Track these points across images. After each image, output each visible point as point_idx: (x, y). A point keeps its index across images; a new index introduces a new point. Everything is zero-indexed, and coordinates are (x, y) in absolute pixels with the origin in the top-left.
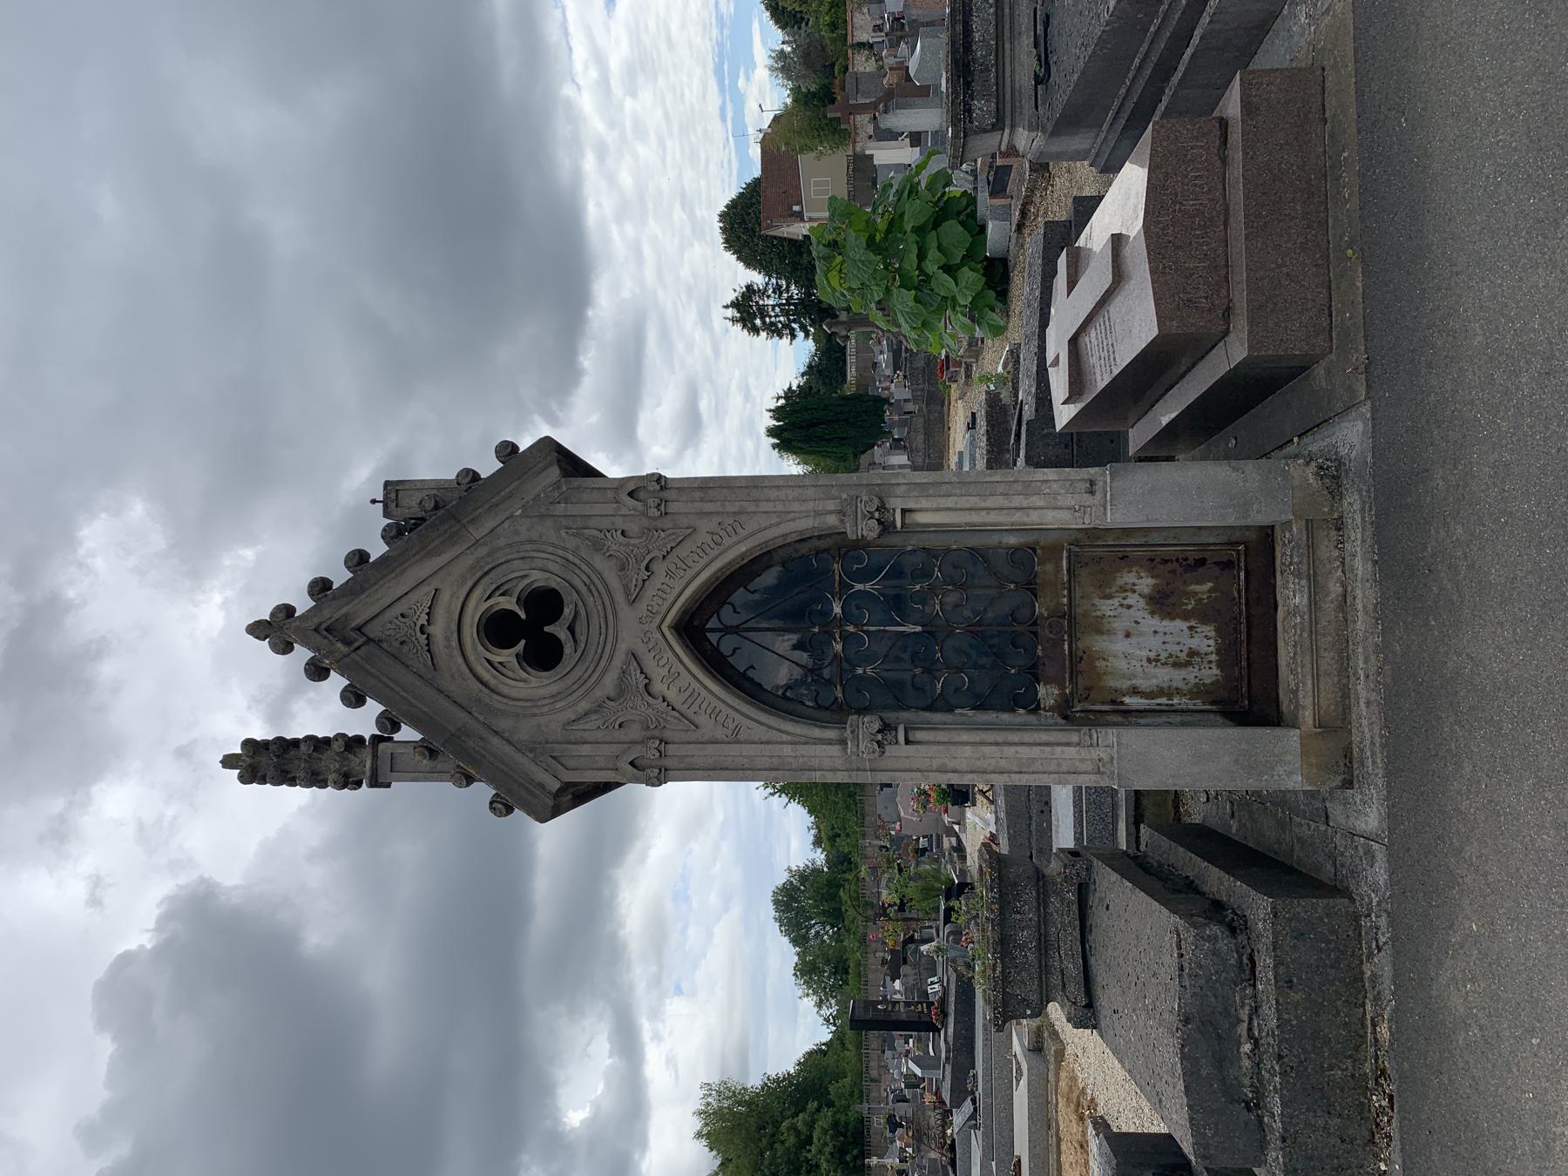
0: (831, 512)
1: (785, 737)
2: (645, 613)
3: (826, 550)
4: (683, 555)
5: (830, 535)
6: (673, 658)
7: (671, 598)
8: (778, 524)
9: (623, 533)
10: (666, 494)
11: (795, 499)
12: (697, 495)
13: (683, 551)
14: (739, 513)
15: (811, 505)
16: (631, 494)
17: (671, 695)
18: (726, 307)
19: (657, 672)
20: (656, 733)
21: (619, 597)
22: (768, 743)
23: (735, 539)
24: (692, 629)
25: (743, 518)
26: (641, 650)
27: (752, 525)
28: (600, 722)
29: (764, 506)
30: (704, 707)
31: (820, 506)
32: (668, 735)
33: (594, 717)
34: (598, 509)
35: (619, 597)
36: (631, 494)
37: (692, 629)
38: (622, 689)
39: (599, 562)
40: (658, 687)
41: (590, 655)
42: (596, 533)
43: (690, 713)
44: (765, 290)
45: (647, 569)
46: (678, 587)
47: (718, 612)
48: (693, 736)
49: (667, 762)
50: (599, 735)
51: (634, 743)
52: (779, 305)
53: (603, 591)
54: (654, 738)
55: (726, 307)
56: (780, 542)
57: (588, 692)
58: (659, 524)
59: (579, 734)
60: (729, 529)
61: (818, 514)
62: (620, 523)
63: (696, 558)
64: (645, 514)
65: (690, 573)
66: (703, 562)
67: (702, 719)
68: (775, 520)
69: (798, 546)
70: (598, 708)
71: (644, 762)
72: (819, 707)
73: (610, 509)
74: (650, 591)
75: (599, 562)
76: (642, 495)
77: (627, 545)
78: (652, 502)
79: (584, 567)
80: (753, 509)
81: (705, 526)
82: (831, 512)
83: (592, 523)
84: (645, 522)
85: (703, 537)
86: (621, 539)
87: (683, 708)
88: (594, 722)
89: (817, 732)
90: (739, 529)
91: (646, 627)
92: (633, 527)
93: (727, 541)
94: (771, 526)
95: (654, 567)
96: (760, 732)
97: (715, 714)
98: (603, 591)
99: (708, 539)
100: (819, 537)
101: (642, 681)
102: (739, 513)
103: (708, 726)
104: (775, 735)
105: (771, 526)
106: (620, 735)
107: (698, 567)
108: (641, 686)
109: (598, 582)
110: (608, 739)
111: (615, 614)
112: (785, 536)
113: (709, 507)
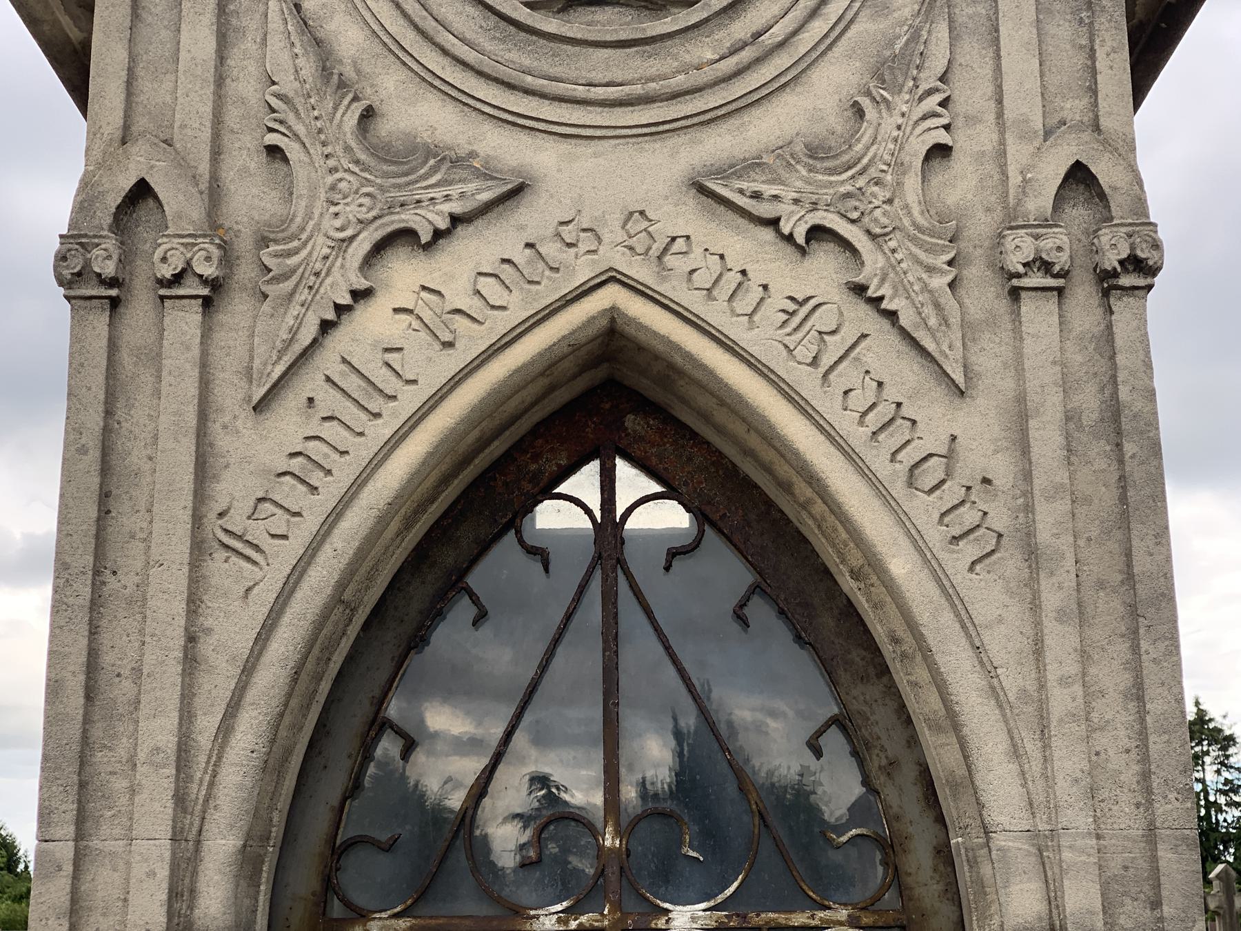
0: (1053, 899)
1: (207, 724)
2: (664, 230)
3: (896, 877)
4: (870, 354)
5: (952, 892)
6: (501, 324)
7: (715, 314)
8: (995, 692)
9: (940, 152)
10: (1083, 293)
11: (1096, 760)
12: (1089, 401)
13: (883, 353)
14: (1032, 554)
15: (1077, 818)
16: (1079, 175)
17: (374, 322)
18: (1197, 704)
19: (457, 268)
20: (245, 272)
21: (718, 145)
22: (191, 661)
23: (935, 536)
24: (611, 395)
25: (1011, 562)
26: (533, 218)
27: (989, 597)
28: (287, 85)
29: (1061, 642)
30: (331, 431)
31: (1076, 854)
32: (237, 311)
33: (308, 68)
34: (1020, 65)
35: (718, 145)
36: (1079, 175)
37: (611, 395)
38: (412, 158)
39: (835, 79)
40: (404, 275)
41: (515, 57)
42: (937, 64)
43: (310, 383)
44: (1228, 767)
45: (817, 233)
46: (762, 335)
47: (671, 493)
48: (231, 395)
49: (140, 308)
50: (245, 85)
51: (215, 194)
52: (1205, 791)
53: (738, 88)
54: (227, 256)
55: (1197, 704)
56: (922, 704)
57: (395, 51)
58: (976, 271)
59: (251, 23)
60: (969, 516)
61: (1044, 845)
62: (972, 142)
63: (859, 401)
64: (1011, 221)
65: (806, 382)
66: (846, 423)
67: (288, 425)
68: (1013, 680)
69: (909, 773)
70: (333, 77)
71: (144, 234)
72: (337, 852)
73: (1024, 104)
74: (745, 247)
75: (835, 79)
76: (1079, 213)
77: (900, 167)
78: (1059, 244)
79: (818, 28)
80: (1052, 599)
81: (977, 429)
82: (1053, 899)
83: (973, 53)
84: (981, 226)
85: (937, 420)
86: (919, 146)
87: (328, 360)
88: (289, 63)
89: (222, 845)
90: (970, 551)
91: (612, 233)
92: (961, 184)
93: (924, 510)
94: (989, 669)
95: (825, 260)
96: (231, 629)
97: (302, 468)
98: (738, 88)
99: (931, 440)
100: (944, 854)
101: (425, 220)
102: (1032, 554)
103: (255, 448)
104: (217, 684)
105: (989, 669)
106: (243, 156)
107: (828, 405)
108: (407, 218)
109: (766, 72)
110: (233, 116)
111: (656, 131)
112: (952, 722)
113: (1047, 439)
